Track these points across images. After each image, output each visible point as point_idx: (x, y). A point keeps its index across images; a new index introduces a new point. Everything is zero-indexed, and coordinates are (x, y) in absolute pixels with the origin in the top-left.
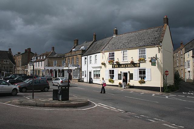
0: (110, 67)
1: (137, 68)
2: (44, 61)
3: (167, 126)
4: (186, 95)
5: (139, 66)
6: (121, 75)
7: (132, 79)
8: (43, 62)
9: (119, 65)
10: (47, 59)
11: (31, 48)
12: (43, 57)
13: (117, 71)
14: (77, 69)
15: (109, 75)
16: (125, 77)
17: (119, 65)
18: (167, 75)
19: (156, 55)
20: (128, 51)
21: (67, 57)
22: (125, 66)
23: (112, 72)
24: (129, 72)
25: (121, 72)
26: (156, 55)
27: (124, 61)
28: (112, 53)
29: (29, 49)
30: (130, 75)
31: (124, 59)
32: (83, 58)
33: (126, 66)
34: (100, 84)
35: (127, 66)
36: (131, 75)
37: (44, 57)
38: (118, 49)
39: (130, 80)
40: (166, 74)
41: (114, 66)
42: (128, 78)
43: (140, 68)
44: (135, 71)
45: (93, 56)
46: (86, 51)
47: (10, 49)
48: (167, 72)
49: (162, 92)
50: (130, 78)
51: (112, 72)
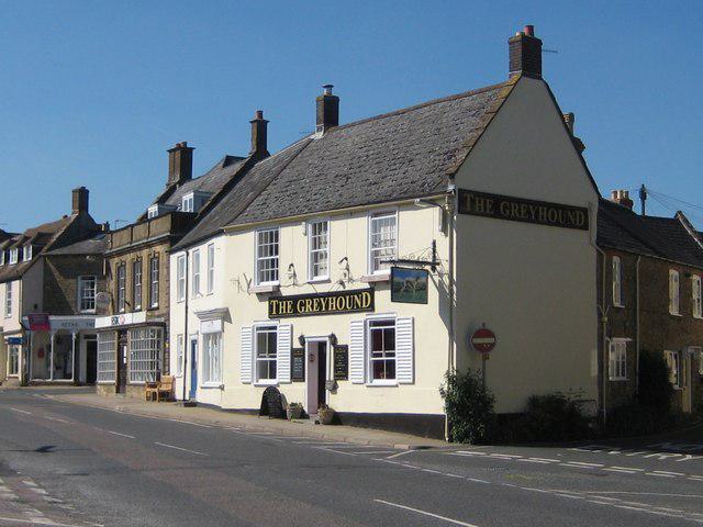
1: (362, 316)
2: (19, 278)
5: (372, 308)
8: (16, 285)
10: (42, 259)
11: (315, 99)
12: (20, 257)
14: (147, 324)
16: (323, 363)
17: (295, 306)
18: (485, 350)
19: (434, 243)
21: (111, 256)
22: (320, 304)
23: (267, 342)
24: (333, 338)
25: (302, 339)
26: (434, 243)
27: (316, 279)
28: (271, 233)
29: (185, 143)
30: (336, 354)
31: (316, 267)
32: (174, 258)
36: (342, 354)
37: (28, 258)
38: (347, 209)
39: (336, 380)
40: (480, 348)
42: (330, 374)
43: (375, 316)
44: (350, 330)
45: (203, 249)
46: (199, 221)
47: (531, 28)
48: (485, 332)
49: (451, 440)
50: (336, 370)
51: (267, 342)
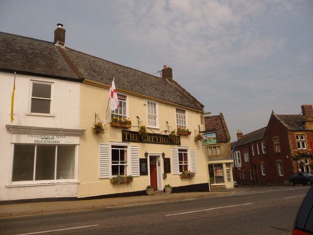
0: (114, 138)
3: (243, 203)
4: (140, 233)
5: (179, 144)
6: (146, 160)
7: (169, 172)
9: (141, 137)
13: (135, 152)
15: (55, 181)
17: (141, 137)
20: (22, 136)
22: (155, 139)
23: (118, 154)
24: (163, 155)
25: (146, 154)
33: (158, 139)
34: (75, 199)
35: (159, 140)
41: (129, 136)
44: (171, 152)
51: (118, 154)
